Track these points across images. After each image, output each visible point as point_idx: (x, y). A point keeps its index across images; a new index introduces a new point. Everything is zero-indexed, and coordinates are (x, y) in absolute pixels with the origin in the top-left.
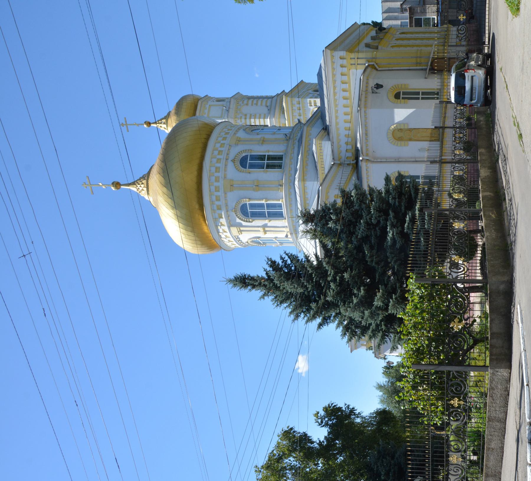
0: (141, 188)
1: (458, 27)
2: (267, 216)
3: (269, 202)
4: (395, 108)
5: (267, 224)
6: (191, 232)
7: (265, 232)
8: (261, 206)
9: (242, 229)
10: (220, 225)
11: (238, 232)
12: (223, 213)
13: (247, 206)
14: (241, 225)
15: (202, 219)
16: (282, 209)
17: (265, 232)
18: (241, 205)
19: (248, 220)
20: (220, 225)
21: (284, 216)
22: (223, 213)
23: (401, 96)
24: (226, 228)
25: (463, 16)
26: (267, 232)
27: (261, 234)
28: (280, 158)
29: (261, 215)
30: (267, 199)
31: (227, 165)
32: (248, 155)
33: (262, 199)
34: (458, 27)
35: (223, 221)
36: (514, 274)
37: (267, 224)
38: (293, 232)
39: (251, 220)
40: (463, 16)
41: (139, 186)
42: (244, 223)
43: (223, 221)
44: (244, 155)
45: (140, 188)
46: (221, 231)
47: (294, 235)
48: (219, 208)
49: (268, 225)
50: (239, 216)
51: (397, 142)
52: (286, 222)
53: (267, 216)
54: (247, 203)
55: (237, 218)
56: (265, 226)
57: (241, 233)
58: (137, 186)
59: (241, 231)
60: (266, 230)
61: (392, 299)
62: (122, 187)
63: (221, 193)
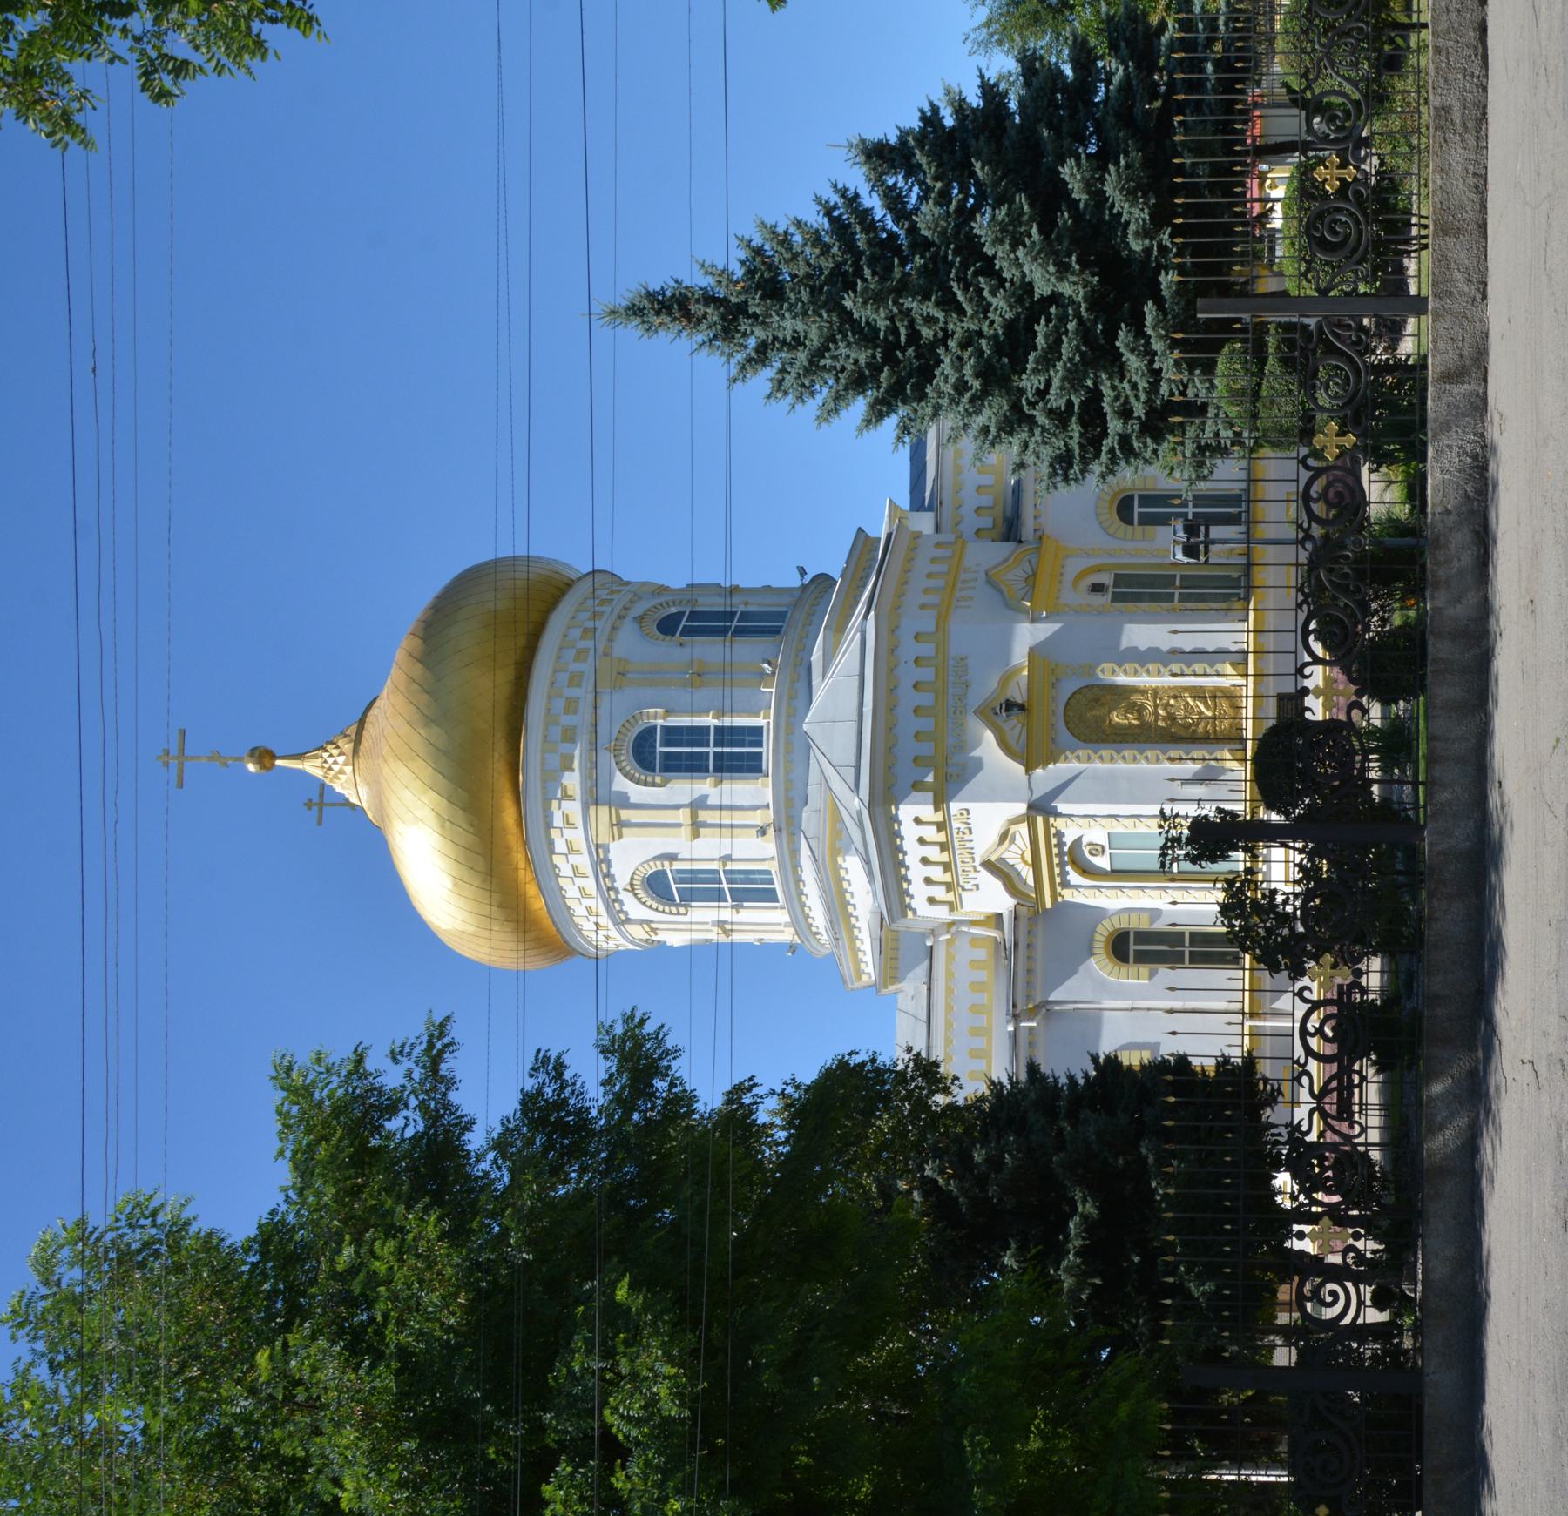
0: (336, 768)
1: (1301, 1285)
2: (711, 768)
3: (727, 721)
4: (1130, 622)
5: (707, 797)
6: (464, 809)
7: (696, 827)
8: (697, 735)
9: (626, 814)
10: (559, 795)
11: (613, 825)
12: (577, 753)
13: (655, 758)
14: (623, 801)
15: (503, 784)
16: (761, 746)
17: (696, 827)
18: (637, 730)
19: (650, 779)
20: (559, 795)
21: (764, 767)
22: (577, 753)
23: (1133, 947)
24: (573, 808)
25: (1341, 434)
26: (701, 830)
27: (678, 842)
28: (781, 616)
29: (693, 766)
30: (721, 713)
31: (618, 628)
32: (684, 613)
33: (706, 712)
34: (1301, 1285)
35: (572, 781)
36: (1494, 799)
37: (707, 797)
38: (783, 826)
39: (658, 780)
40: (1341, 434)
41: (330, 760)
42: (636, 792)
43: (572, 781)
44: (674, 610)
45: (334, 766)
46: (558, 821)
47: (784, 835)
48: (570, 736)
49: (710, 802)
50: (624, 764)
51: (1117, 968)
52: (765, 786)
53: (711, 768)
54: (655, 728)
55: (618, 772)
56: (698, 804)
57: (620, 836)
58: (325, 762)
59: (620, 825)
60: (700, 819)
61: (1117, 164)
62: (279, 762)
63: (584, 693)
